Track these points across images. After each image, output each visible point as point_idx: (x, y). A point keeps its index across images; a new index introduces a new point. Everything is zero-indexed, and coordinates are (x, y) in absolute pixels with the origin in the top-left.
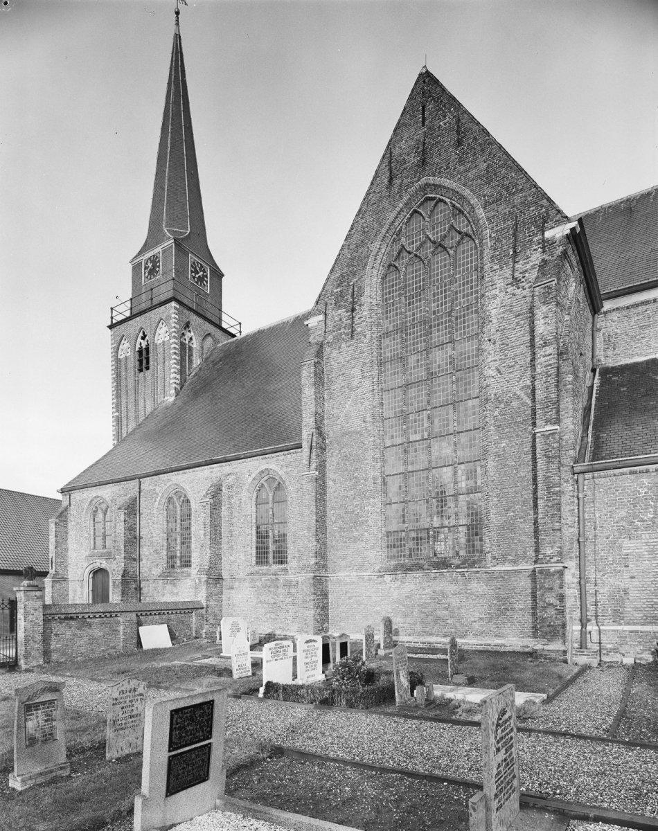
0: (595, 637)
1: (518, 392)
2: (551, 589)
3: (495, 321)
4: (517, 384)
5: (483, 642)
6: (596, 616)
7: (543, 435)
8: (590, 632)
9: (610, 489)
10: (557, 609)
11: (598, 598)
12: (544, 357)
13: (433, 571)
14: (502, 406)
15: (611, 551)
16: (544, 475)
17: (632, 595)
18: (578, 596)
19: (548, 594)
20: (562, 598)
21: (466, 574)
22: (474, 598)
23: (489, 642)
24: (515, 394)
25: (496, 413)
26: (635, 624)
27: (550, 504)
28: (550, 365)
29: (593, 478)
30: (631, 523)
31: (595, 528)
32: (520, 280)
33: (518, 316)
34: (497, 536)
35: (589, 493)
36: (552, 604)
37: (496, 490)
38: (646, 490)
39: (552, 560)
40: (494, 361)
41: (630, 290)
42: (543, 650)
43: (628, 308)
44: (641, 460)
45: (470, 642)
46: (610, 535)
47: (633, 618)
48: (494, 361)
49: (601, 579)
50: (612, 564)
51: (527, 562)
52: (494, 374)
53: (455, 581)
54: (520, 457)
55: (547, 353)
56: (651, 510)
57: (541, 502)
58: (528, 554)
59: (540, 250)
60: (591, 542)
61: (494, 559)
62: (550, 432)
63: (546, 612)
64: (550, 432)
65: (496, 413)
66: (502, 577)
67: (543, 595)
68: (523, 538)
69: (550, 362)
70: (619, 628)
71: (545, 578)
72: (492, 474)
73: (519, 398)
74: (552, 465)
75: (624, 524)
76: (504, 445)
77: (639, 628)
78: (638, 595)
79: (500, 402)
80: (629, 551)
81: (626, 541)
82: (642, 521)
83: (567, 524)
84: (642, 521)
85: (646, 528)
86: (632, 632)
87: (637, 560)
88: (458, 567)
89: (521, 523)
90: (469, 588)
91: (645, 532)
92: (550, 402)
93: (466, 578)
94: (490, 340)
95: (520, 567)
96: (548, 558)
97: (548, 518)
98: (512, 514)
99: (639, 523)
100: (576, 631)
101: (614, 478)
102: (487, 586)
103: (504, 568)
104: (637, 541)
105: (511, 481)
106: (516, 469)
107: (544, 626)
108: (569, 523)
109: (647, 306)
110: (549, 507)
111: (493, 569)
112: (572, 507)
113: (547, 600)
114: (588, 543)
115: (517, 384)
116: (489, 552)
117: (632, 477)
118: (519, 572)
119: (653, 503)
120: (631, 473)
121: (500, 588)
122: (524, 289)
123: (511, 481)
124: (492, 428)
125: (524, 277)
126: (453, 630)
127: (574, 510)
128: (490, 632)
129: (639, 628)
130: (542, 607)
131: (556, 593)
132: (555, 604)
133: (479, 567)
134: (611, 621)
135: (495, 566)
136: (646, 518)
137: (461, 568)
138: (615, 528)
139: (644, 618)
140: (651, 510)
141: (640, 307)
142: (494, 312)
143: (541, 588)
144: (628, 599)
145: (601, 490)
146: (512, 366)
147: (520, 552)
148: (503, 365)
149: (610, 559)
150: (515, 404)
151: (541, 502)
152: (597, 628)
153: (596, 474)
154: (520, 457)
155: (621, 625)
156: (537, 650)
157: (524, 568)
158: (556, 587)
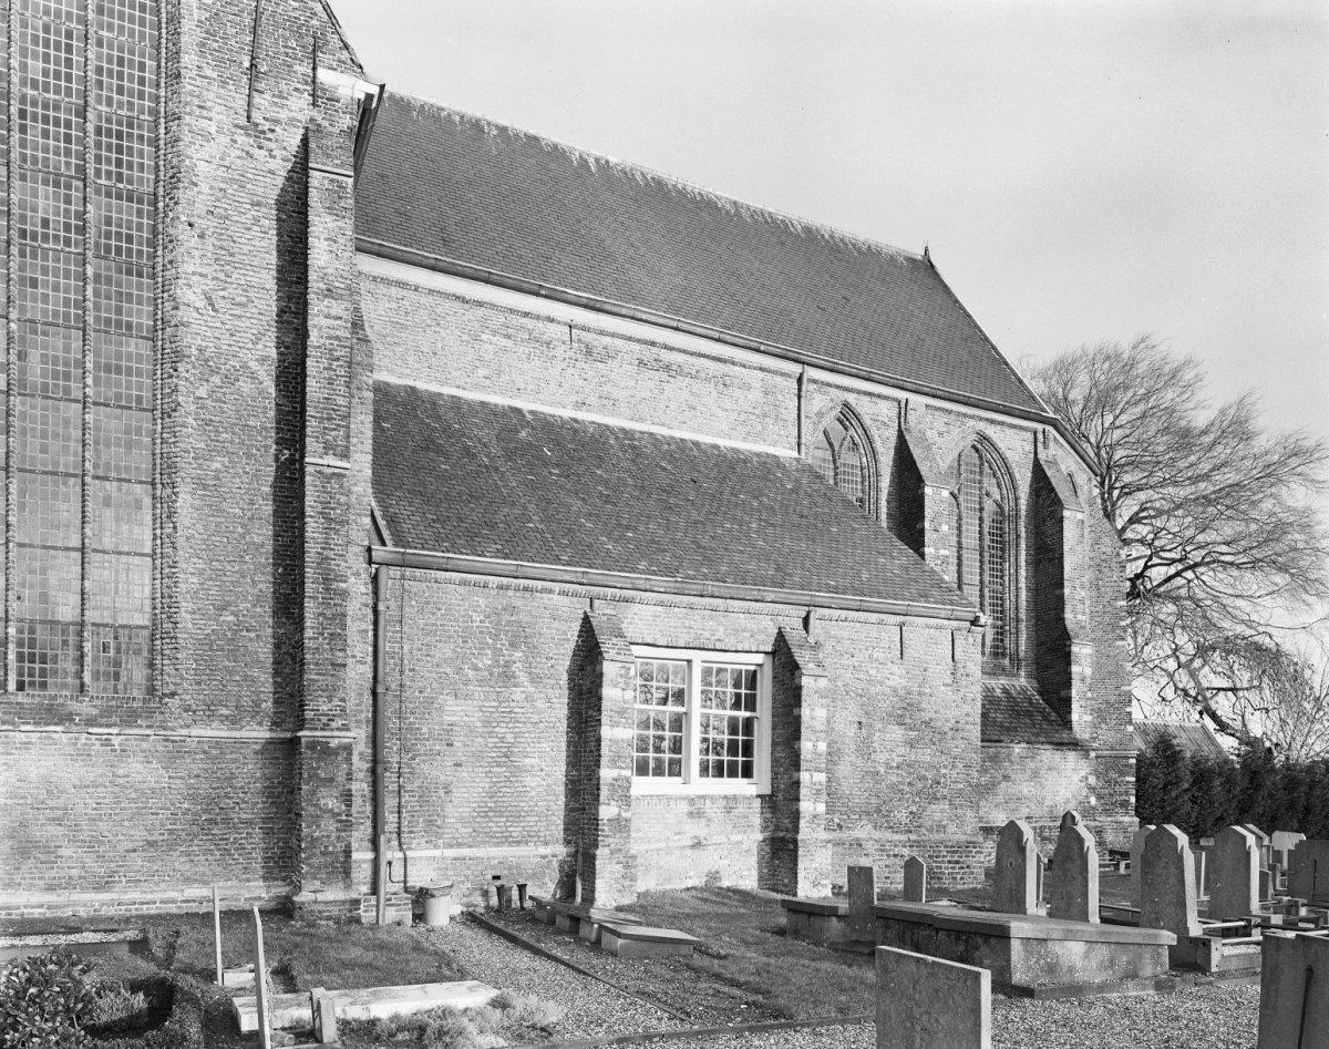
0: (397, 873)
1: (254, 365)
2: (332, 780)
3: (204, 188)
4: (250, 346)
5: (157, 896)
6: (399, 834)
7: (319, 472)
8: (390, 863)
9: (427, 603)
10: (341, 821)
11: (403, 800)
12: (326, 317)
13: (23, 728)
14: (216, 380)
15: (427, 716)
16: (319, 553)
17: (459, 795)
18: (369, 795)
19: (324, 792)
20: (347, 798)
21: (116, 741)
22: (133, 795)
23: (172, 895)
24: (245, 366)
25: (202, 392)
26: (460, 845)
27: (328, 612)
28: (337, 338)
29: (403, 577)
30: (459, 671)
31: (402, 672)
32: (264, 132)
33: (258, 204)
34: (196, 661)
35: (393, 604)
36: (331, 811)
37: (196, 560)
38: (482, 618)
39: (333, 724)
40: (201, 275)
41: (1027, 415)
42: (316, 902)
43: (375, 278)
44: (479, 564)
45: (125, 897)
46: (425, 688)
47: (458, 836)
48: (201, 275)
49: (410, 766)
50: (428, 740)
51: (260, 724)
52: (199, 304)
53: (85, 754)
54: (252, 502)
55: (333, 312)
56: (489, 652)
57: (312, 605)
58: (264, 705)
59: (306, 95)
60: (394, 696)
61: (186, 711)
62: (333, 470)
63: (318, 826)
64: (333, 470)
65: (202, 392)
66: (205, 752)
67: (314, 793)
68: (255, 672)
69: (338, 333)
70: (437, 853)
71: (319, 759)
72: (187, 522)
73: (253, 377)
74: (336, 537)
75: (448, 670)
76: (218, 465)
77: (465, 852)
78: (466, 795)
79: (213, 372)
80: (455, 719)
81: (451, 700)
82: (476, 669)
83: (354, 656)
84: (476, 669)
85: (481, 682)
86: (455, 859)
87: (466, 735)
88: (91, 722)
89: (251, 640)
90: (120, 772)
91: (480, 689)
92: (333, 409)
93: (114, 751)
94: (191, 225)
95: (244, 734)
96: (325, 720)
97: (325, 639)
98: (232, 618)
99: (471, 672)
100: (364, 861)
101: (435, 585)
102: (166, 768)
103: (210, 733)
104: (467, 702)
105: (229, 548)
106: (244, 526)
107: (314, 854)
108: (359, 655)
109: (405, 293)
110: (326, 618)
111: (184, 732)
112: (364, 627)
113: (322, 802)
114: (389, 697)
115: (250, 346)
116: (173, 694)
117: (462, 590)
118: (244, 743)
119: (490, 641)
120: (463, 583)
121: (198, 776)
122: (272, 156)
123: (229, 548)
124: (190, 420)
125: (273, 131)
126: (74, 872)
127: (367, 631)
128: (172, 873)
129: (465, 852)
130: (312, 816)
131: (340, 789)
132: (336, 811)
133: (148, 727)
134: (423, 840)
135: (188, 726)
136: (480, 665)
137: (101, 726)
138: (434, 675)
139: (474, 834)
140: (489, 652)
141: (393, 288)
142: (202, 167)
143: (310, 777)
144: (451, 801)
145: (413, 603)
146: (239, 304)
147: (246, 702)
148: (222, 293)
149: (425, 730)
150: (246, 386)
151: (312, 605)
152: (401, 855)
153: (408, 572)
154: (252, 502)
155: (436, 847)
156: (303, 903)
157: (254, 734)
158: (341, 777)
